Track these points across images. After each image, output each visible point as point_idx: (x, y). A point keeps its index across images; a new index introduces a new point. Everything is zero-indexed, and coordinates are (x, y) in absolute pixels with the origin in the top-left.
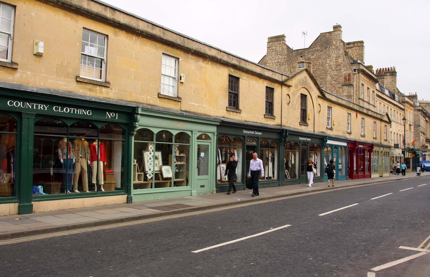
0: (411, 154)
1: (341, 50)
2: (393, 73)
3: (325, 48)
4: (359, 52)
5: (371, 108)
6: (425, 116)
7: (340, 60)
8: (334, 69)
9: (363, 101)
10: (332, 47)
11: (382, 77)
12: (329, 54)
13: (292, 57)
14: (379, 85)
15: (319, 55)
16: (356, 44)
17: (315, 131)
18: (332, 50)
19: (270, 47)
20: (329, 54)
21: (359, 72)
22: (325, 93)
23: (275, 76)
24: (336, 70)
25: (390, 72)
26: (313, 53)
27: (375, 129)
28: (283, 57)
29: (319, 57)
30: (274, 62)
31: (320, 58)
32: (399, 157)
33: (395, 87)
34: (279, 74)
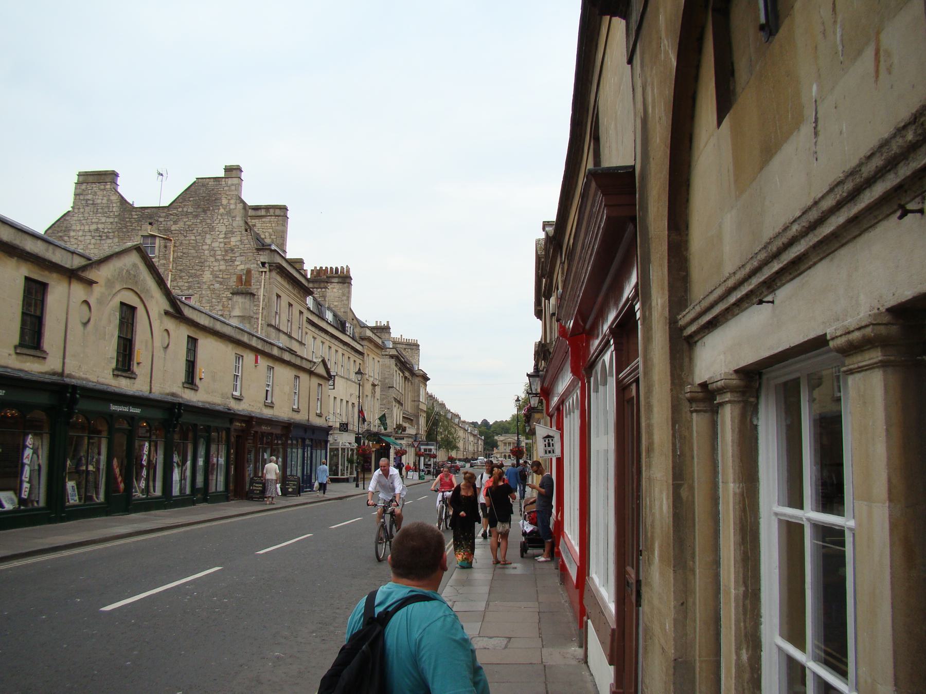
0: (373, 444)
1: (237, 219)
2: (344, 278)
3: (204, 211)
4: (277, 228)
5: (295, 346)
6: (402, 368)
7: (234, 240)
8: (219, 257)
9: (278, 332)
10: (219, 209)
11: (322, 285)
12: (213, 225)
13: (131, 222)
14: (315, 299)
15: (191, 223)
16: (272, 211)
17: (153, 391)
18: (219, 217)
19: (82, 194)
20: (213, 225)
21: (272, 268)
22: (182, 306)
23: (53, 253)
24: (224, 259)
25: (339, 277)
26: (177, 217)
27: (297, 392)
28: (108, 220)
29: (190, 229)
30: (87, 228)
31: (192, 230)
32: (348, 449)
33: (348, 308)
34: (63, 251)
